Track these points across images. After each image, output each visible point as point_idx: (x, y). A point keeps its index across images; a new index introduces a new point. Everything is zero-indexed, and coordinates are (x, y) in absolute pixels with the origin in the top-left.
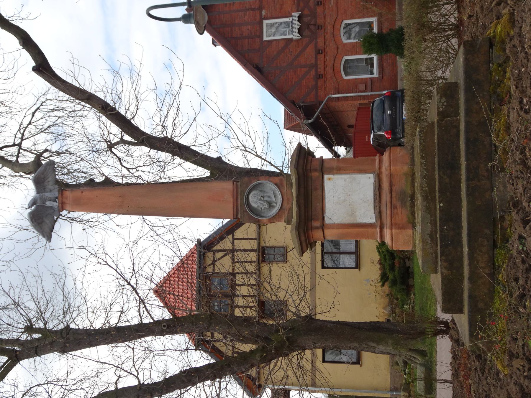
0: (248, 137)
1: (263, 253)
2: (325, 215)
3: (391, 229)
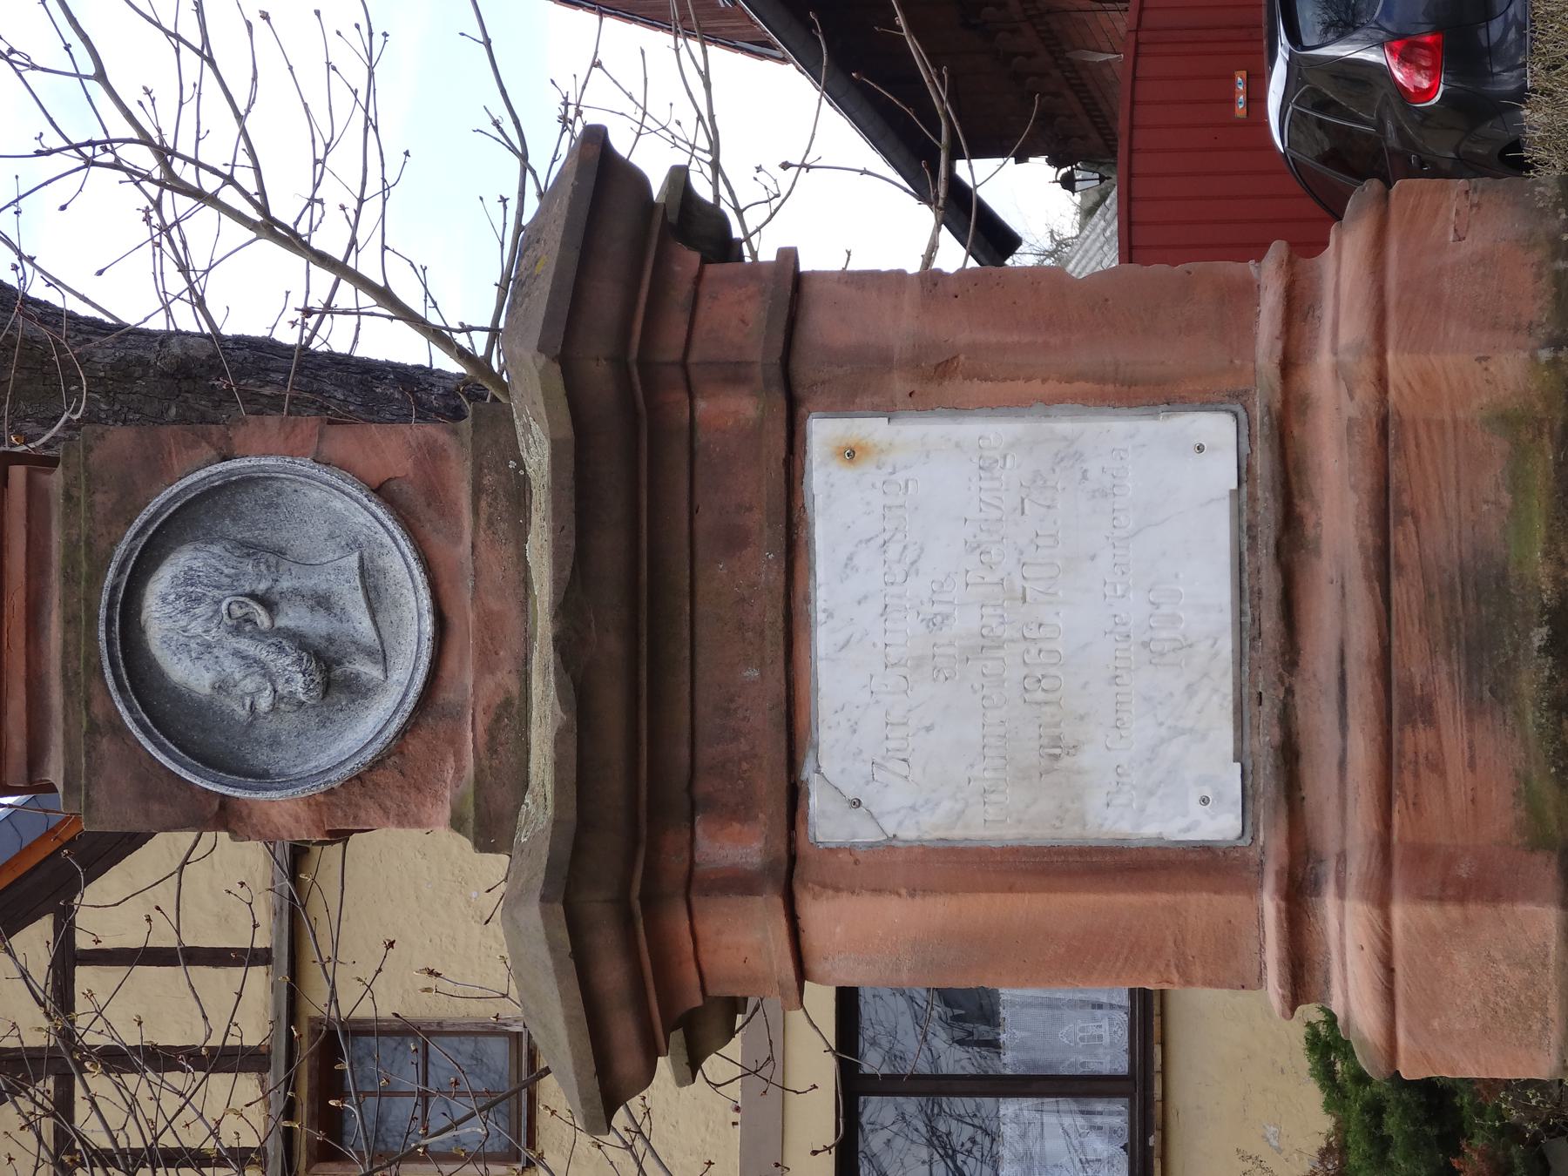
0: (191, 60)
1: (329, 1083)
2: (807, 772)
3: (1383, 902)
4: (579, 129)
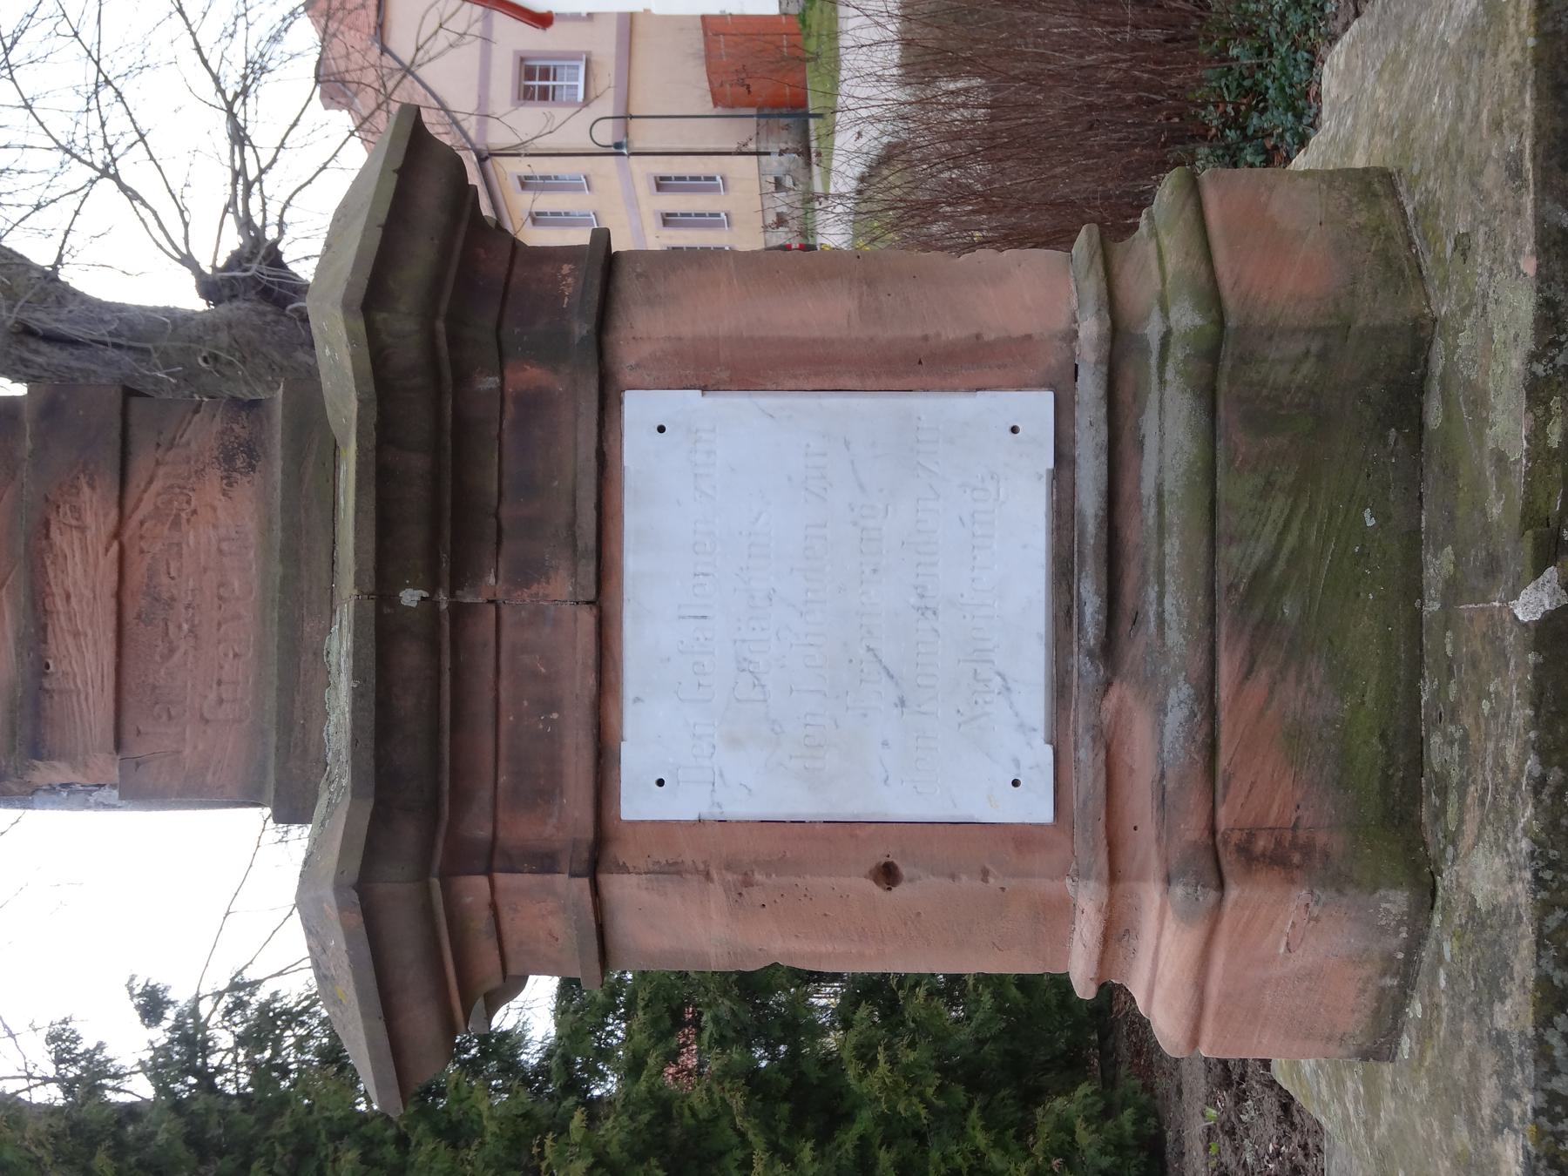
4: (395, 107)
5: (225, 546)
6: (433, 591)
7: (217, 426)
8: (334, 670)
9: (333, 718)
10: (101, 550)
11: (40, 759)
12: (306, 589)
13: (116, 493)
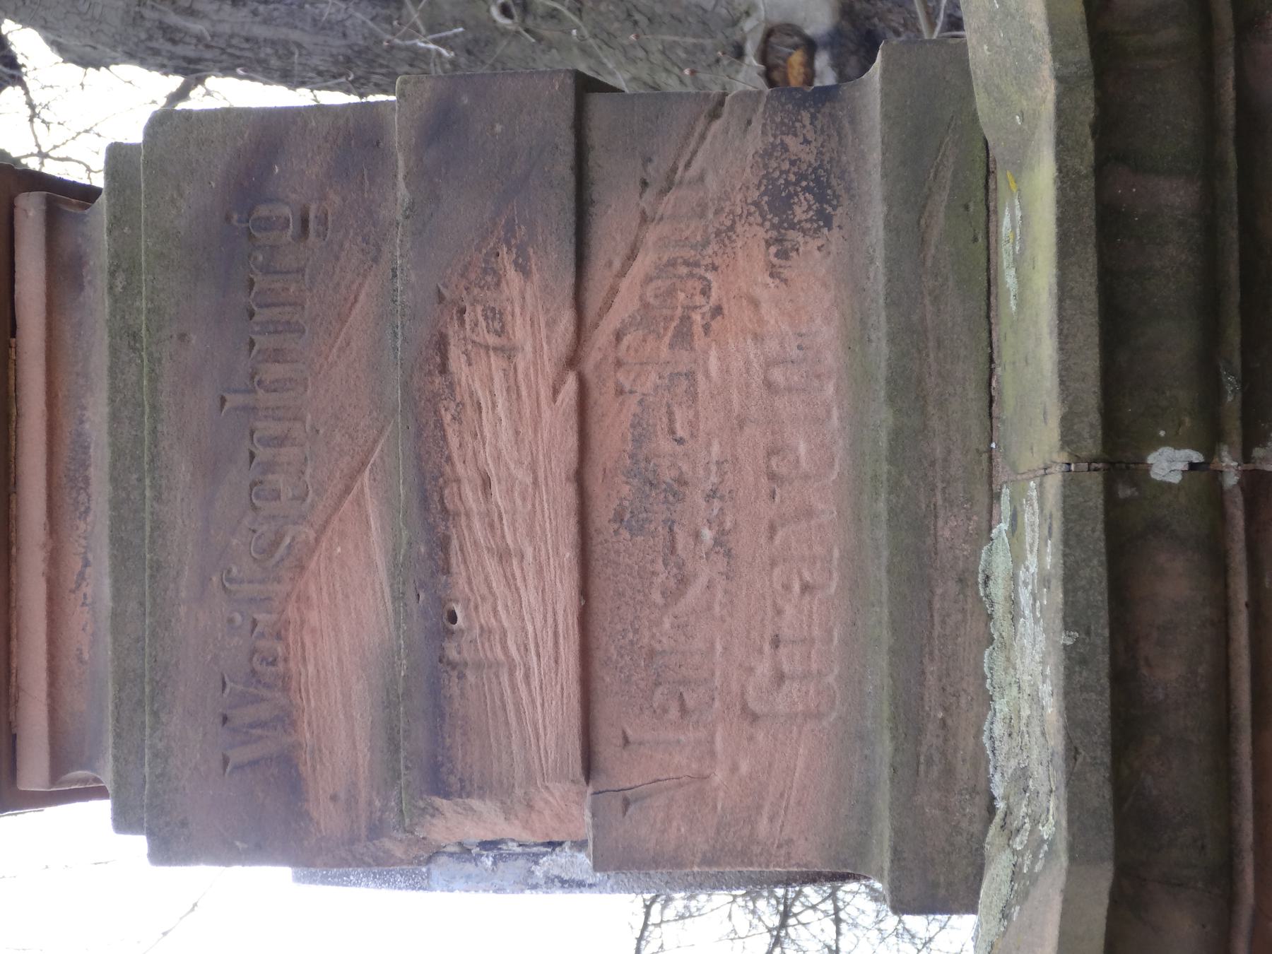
5: (777, 375)
6: (1210, 452)
7: (755, 141)
8: (1000, 610)
9: (1001, 706)
10: (545, 393)
11: (447, 796)
12: (939, 453)
13: (569, 280)
